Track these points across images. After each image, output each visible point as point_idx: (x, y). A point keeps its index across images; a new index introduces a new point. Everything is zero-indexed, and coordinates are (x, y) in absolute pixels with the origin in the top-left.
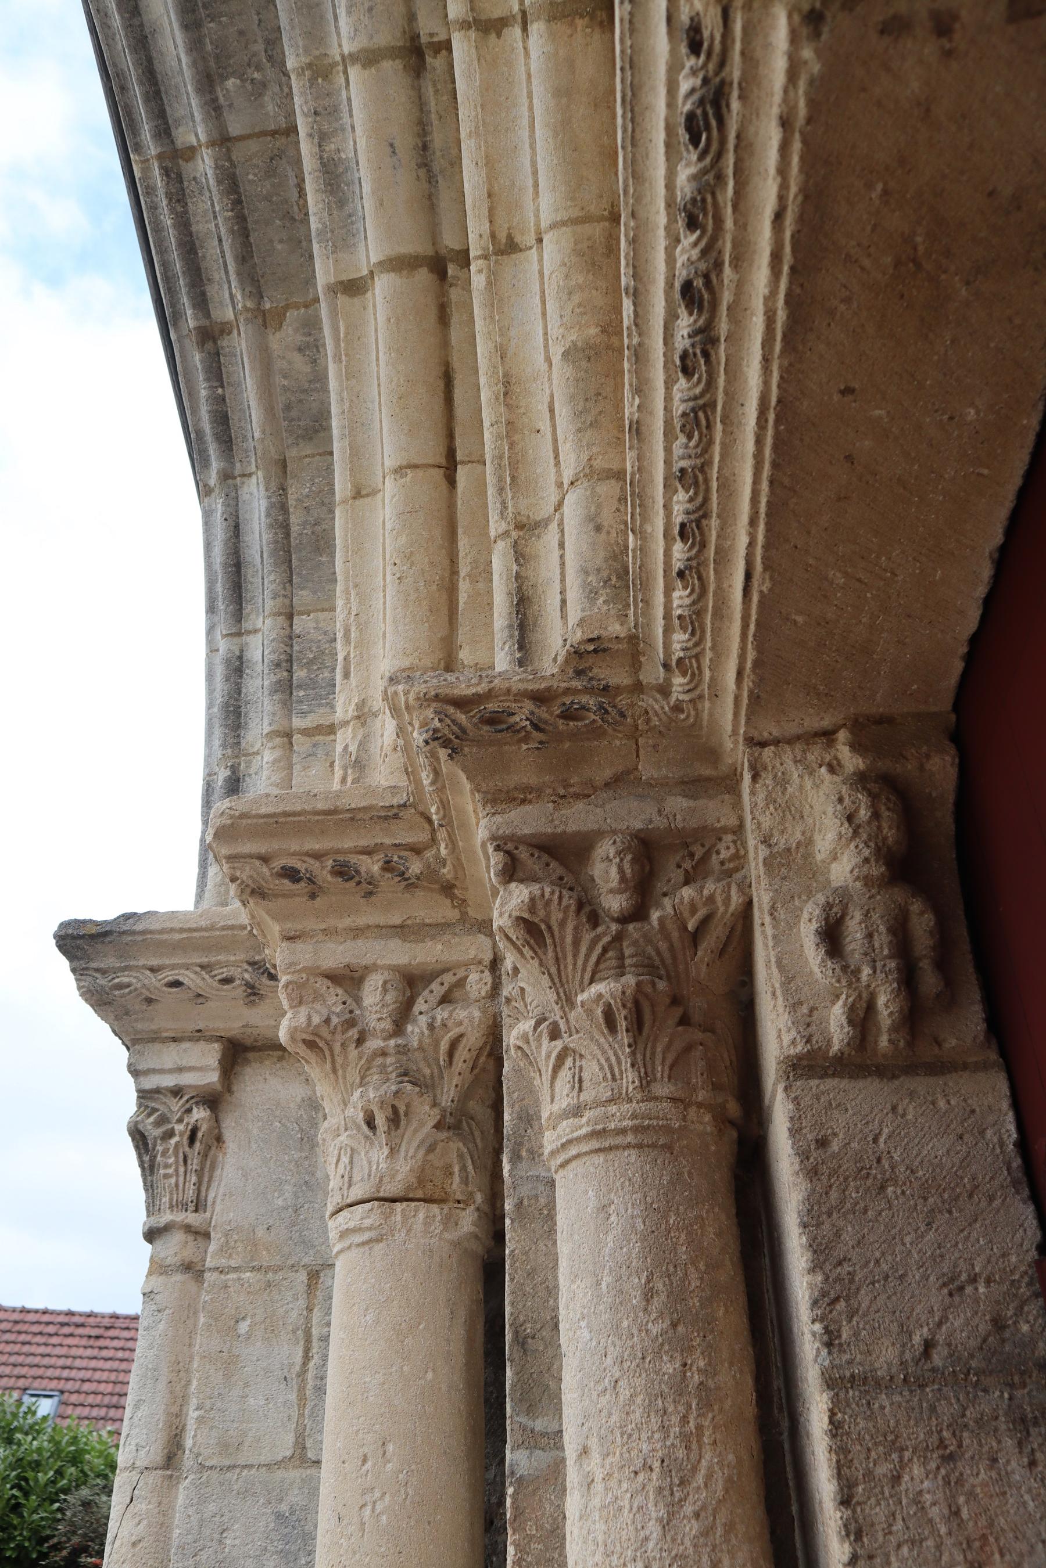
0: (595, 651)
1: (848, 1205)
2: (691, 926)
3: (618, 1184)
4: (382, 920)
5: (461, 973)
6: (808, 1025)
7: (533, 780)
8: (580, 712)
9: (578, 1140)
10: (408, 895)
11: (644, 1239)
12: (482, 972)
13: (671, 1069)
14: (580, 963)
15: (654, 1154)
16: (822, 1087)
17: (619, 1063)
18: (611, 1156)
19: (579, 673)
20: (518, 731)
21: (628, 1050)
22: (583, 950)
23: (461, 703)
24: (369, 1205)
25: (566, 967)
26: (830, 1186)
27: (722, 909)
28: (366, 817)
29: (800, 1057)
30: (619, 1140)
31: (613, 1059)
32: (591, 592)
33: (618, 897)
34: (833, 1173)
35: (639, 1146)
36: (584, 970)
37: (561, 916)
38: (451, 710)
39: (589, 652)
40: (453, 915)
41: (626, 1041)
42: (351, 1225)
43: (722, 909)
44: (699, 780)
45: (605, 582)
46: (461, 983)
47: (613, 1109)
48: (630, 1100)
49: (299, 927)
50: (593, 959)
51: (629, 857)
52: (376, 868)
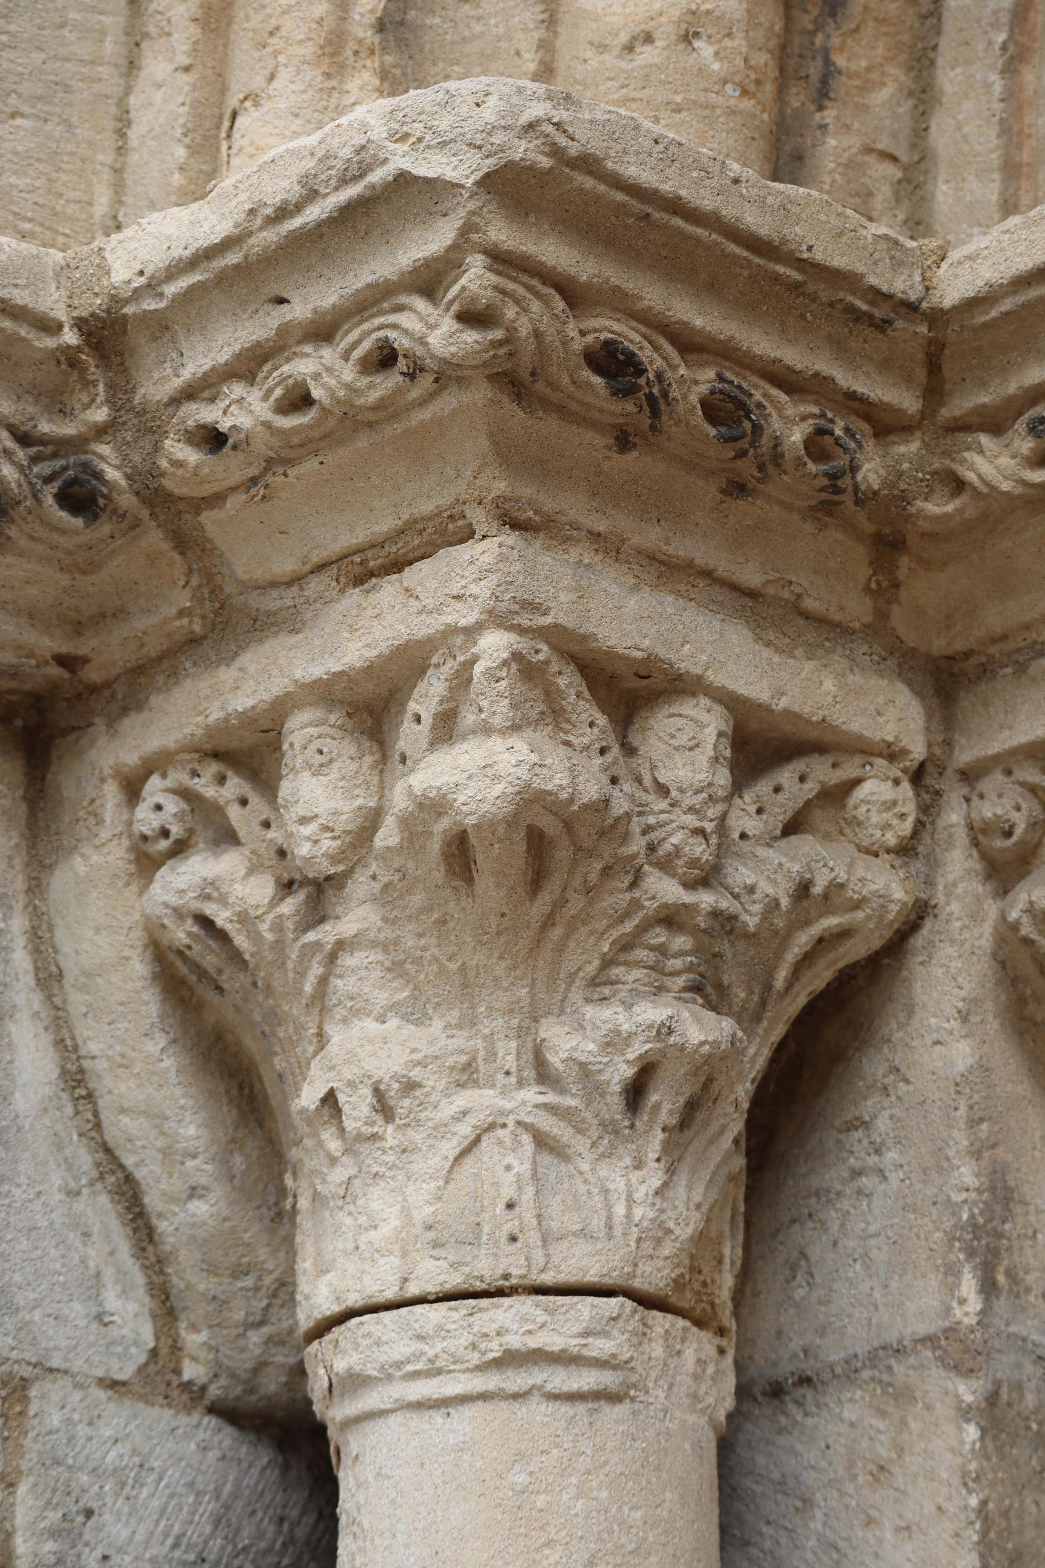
4: (722, 564)
5: (849, 770)
10: (809, 527)
24: (613, 1304)
28: (825, 296)
40: (858, 609)
42: (554, 1342)
46: (836, 795)
49: (550, 506)
52: (796, 436)
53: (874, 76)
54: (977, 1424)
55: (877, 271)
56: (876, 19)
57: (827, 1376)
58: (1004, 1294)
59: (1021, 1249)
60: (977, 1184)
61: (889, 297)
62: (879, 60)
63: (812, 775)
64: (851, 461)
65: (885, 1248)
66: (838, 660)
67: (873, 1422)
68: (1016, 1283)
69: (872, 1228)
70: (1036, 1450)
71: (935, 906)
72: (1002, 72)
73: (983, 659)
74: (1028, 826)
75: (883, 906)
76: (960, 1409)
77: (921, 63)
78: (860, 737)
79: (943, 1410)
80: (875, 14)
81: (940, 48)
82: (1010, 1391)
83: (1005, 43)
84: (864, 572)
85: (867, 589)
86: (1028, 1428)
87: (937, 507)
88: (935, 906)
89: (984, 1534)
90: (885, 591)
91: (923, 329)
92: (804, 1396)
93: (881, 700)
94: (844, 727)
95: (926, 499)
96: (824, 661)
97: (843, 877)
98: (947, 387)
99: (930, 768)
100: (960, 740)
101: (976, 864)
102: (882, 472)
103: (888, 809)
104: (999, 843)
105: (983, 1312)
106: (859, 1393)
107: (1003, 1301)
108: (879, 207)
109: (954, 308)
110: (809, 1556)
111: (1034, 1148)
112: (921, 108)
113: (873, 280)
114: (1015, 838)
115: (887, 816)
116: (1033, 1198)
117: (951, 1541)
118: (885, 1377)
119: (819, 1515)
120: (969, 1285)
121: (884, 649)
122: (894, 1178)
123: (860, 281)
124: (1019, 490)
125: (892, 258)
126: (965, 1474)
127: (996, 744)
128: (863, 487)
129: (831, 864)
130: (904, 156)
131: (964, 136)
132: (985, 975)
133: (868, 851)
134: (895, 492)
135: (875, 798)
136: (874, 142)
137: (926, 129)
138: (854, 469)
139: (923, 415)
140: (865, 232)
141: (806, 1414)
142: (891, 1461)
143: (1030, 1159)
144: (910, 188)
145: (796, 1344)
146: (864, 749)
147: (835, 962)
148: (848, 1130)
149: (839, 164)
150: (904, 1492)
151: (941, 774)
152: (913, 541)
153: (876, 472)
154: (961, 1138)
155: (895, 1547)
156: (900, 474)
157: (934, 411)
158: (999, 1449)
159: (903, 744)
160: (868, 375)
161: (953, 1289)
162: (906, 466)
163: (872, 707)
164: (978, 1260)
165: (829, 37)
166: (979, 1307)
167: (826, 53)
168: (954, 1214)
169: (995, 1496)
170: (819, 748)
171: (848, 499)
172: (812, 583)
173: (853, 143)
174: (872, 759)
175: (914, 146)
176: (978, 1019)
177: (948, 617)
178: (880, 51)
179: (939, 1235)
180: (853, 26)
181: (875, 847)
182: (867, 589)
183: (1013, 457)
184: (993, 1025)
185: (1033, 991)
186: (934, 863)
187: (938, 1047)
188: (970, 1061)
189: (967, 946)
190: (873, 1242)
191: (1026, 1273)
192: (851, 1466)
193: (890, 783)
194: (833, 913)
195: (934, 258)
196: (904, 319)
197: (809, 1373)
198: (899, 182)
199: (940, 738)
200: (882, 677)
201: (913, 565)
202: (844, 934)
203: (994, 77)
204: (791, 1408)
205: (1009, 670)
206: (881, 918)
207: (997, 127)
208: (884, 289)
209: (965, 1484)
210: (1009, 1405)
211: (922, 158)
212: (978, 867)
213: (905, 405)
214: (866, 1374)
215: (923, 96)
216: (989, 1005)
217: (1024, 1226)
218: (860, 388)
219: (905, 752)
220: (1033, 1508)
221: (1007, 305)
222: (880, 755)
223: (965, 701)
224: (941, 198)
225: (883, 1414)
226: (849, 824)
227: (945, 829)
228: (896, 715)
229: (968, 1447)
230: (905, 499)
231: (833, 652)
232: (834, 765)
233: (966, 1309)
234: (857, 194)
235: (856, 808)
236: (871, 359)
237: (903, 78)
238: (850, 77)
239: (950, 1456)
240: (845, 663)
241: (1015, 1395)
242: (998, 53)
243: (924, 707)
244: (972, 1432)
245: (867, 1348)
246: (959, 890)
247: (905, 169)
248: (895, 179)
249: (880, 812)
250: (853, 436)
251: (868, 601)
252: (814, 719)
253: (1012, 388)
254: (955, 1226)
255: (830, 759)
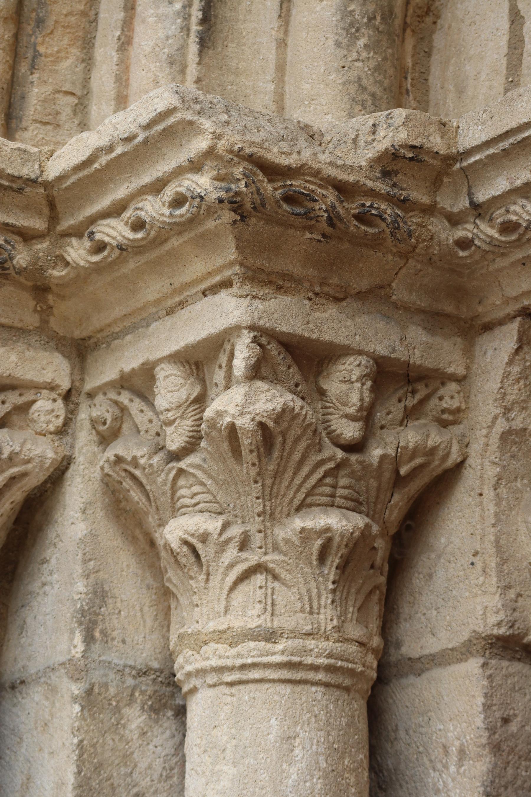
0: (411, 159)
1: (519, 783)
2: (403, 471)
3: (305, 718)
5: (28, 397)
6: (514, 610)
7: (296, 270)
8: (373, 218)
9: (267, 666)
11: (326, 777)
12: (54, 400)
13: (359, 609)
14: (297, 481)
15: (337, 693)
16: (510, 669)
17: (319, 597)
18: (299, 688)
19: (386, 174)
20: (311, 219)
21: (331, 586)
22: (305, 470)
23: (273, 171)
25: (281, 482)
26: (508, 763)
27: (437, 463)
29: (499, 638)
30: (311, 675)
31: (314, 592)
32: (352, 25)
33: (352, 424)
34: (512, 750)
35: (327, 685)
36: (298, 490)
37: (299, 432)
38: (261, 176)
39: (404, 157)
40: (32, 320)
41: (332, 577)
43: (437, 463)
44: (437, 314)
45: (370, 19)
46: (24, 409)
47: (311, 643)
48: (327, 639)
50: (313, 480)
51: (369, 384)
53: (62, 54)
54: (80, 704)
55: (13, 166)
56: (63, 27)
57: (30, 680)
58: (98, 642)
59: (110, 620)
60: (85, 590)
61: (20, 178)
62: (65, 46)
63: (8, 400)
64: (9, 255)
65: (52, 620)
66: (20, 346)
67: (44, 702)
68: (106, 636)
69: (48, 610)
70: (114, 714)
71: (74, 458)
72: (117, 51)
73: (96, 340)
74: (113, 420)
75: (41, 461)
76: (72, 697)
77: (87, 44)
78: (32, 381)
79: (67, 698)
80: (62, 24)
81: (97, 38)
82: (100, 688)
83: (119, 36)
84: (32, 303)
85: (35, 311)
86: (110, 704)
87: (58, 273)
88: (74, 458)
89: (80, 756)
90: (45, 312)
91: (41, 190)
92: (22, 689)
93: (45, 362)
94: (22, 377)
95: (53, 269)
96: (12, 347)
97: (17, 449)
98: (60, 215)
99: (74, 392)
100: (87, 378)
101: (94, 437)
102: (28, 258)
103: (50, 413)
104: (101, 428)
105: (85, 651)
106: (40, 688)
107: (97, 645)
108: (64, 119)
109: (53, 180)
110: (21, 764)
111: (123, 571)
112: (88, 67)
113: (10, 171)
114: (107, 426)
115: (49, 417)
116: (120, 594)
117: (66, 759)
118: (49, 682)
119: (24, 745)
120: (78, 639)
121: (48, 337)
122: (56, 586)
123: (3, 172)
124: (87, 265)
125: (21, 159)
126: (73, 728)
127: (99, 381)
128: (17, 267)
129: (11, 443)
130: (79, 93)
131: (102, 82)
132: (96, 490)
133: (40, 434)
134: (36, 267)
135: (41, 409)
136: (61, 87)
137: (90, 78)
138: (12, 259)
139: (49, 229)
140: (6, 148)
141: (23, 698)
142: (49, 721)
143: (119, 576)
144: (82, 107)
145: (20, 665)
146: (37, 387)
147: (22, 488)
148: (42, 564)
149: (39, 101)
150: (52, 736)
151: (79, 395)
152: (54, 288)
153: (24, 259)
154: (79, 569)
155: (48, 761)
156: (38, 259)
157: (55, 227)
158: (92, 716)
159: (57, 382)
160: (16, 214)
161: (72, 640)
162: (41, 254)
163: (39, 366)
164: (83, 627)
165: (36, 38)
166: (83, 649)
167: (35, 45)
168: (74, 605)
169: (88, 738)
170: (13, 387)
171: (12, 271)
172: (4, 310)
173: (48, 89)
174: (40, 391)
175: (84, 87)
176: (91, 511)
177: (80, 320)
178: (66, 41)
179: (69, 615)
180: (49, 32)
181: (44, 432)
182: (35, 311)
183: (84, 250)
184: (100, 514)
185: (124, 496)
186: (74, 437)
187: (73, 526)
188: (85, 532)
189: (86, 477)
190: (48, 617)
191: (113, 631)
192: (36, 723)
193: (50, 401)
194: (16, 466)
195: (46, 156)
196: (31, 187)
197: (24, 678)
198: (76, 105)
199: (78, 378)
200: (46, 351)
201: (55, 299)
202: (24, 475)
203: (114, 53)
204: (18, 694)
205: (104, 346)
206: (41, 467)
207: (114, 79)
208: (16, 174)
209: (73, 733)
210: (99, 694)
211: (88, 93)
212: (96, 438)
213: (37, 226)
214: (42, 680)
215: (88, 61)
216: (99, 504)
217: (113, 609)
218: (10, 221)
219: (58, 386)
220: (111, 742)
221: (73, 179)
222: (45, 388)
223: (90, 359)
224: (93, 113)
225: (47, 698)
226: (31, 421)
227: (80, 421)
228: (55, 368)
229: (74, 715)
230: (42, 269)
231: (18, 342)
232: (21, 395)
233: (77, 650)
234: (50, 114)
235: (33, 414)
236: (18, 206)
237: (79, 54)
238: (46, 57)
239: (68, 719)
240: (25, 346)
241: (103, 689)
242: (116, 41)
243: (70, 364)
244: (77, 708)
245: (43, 668)
246: (84, 451)
247: (79, 99)
248: (74, 104)
249: (45, 415)
250: (9, 243)
251: (37, 316)
252: (4, 375)
253: (81, 218)
254: (74, 611)
255: (17, 392)
